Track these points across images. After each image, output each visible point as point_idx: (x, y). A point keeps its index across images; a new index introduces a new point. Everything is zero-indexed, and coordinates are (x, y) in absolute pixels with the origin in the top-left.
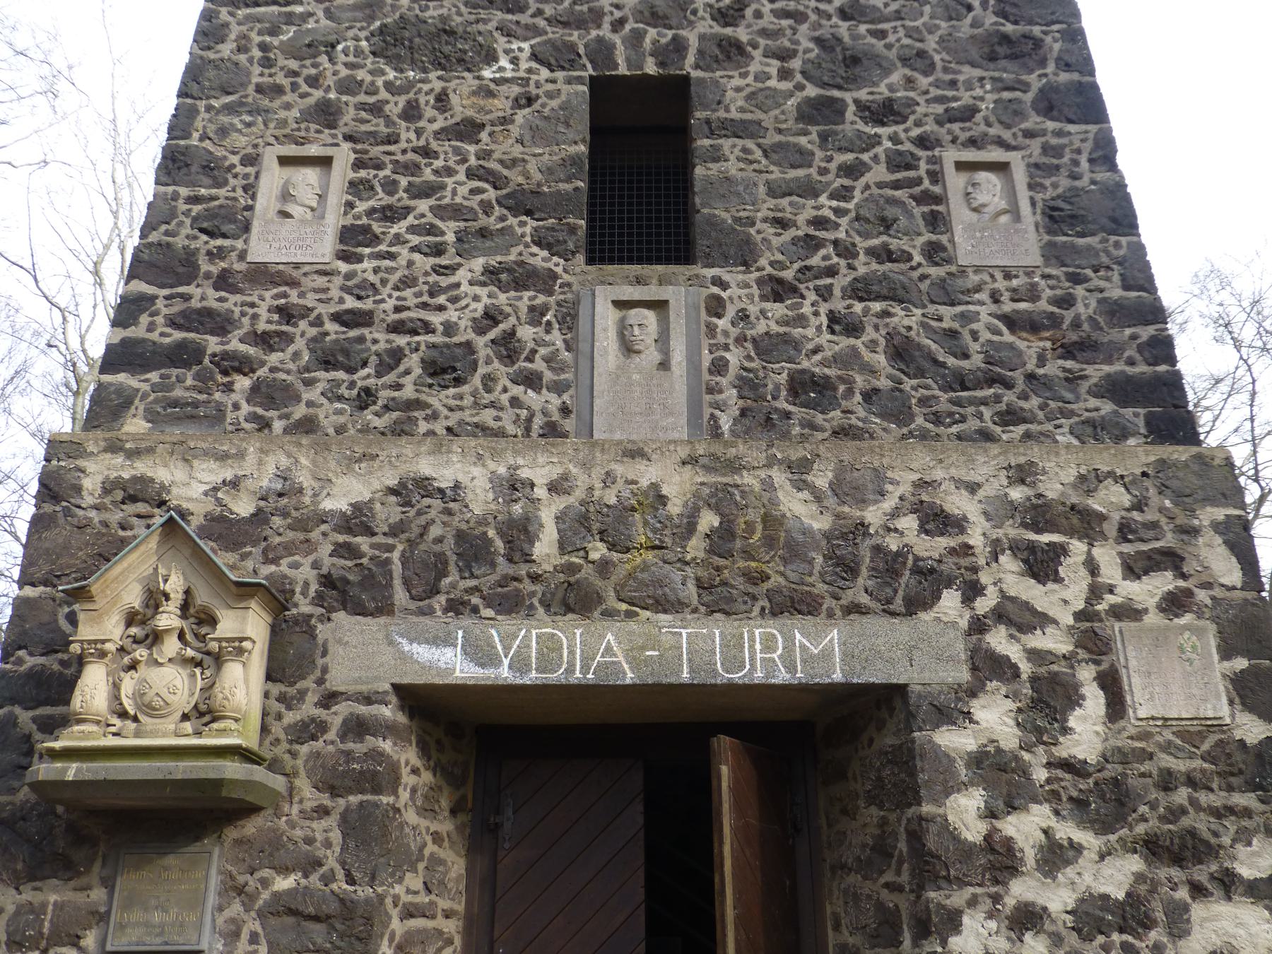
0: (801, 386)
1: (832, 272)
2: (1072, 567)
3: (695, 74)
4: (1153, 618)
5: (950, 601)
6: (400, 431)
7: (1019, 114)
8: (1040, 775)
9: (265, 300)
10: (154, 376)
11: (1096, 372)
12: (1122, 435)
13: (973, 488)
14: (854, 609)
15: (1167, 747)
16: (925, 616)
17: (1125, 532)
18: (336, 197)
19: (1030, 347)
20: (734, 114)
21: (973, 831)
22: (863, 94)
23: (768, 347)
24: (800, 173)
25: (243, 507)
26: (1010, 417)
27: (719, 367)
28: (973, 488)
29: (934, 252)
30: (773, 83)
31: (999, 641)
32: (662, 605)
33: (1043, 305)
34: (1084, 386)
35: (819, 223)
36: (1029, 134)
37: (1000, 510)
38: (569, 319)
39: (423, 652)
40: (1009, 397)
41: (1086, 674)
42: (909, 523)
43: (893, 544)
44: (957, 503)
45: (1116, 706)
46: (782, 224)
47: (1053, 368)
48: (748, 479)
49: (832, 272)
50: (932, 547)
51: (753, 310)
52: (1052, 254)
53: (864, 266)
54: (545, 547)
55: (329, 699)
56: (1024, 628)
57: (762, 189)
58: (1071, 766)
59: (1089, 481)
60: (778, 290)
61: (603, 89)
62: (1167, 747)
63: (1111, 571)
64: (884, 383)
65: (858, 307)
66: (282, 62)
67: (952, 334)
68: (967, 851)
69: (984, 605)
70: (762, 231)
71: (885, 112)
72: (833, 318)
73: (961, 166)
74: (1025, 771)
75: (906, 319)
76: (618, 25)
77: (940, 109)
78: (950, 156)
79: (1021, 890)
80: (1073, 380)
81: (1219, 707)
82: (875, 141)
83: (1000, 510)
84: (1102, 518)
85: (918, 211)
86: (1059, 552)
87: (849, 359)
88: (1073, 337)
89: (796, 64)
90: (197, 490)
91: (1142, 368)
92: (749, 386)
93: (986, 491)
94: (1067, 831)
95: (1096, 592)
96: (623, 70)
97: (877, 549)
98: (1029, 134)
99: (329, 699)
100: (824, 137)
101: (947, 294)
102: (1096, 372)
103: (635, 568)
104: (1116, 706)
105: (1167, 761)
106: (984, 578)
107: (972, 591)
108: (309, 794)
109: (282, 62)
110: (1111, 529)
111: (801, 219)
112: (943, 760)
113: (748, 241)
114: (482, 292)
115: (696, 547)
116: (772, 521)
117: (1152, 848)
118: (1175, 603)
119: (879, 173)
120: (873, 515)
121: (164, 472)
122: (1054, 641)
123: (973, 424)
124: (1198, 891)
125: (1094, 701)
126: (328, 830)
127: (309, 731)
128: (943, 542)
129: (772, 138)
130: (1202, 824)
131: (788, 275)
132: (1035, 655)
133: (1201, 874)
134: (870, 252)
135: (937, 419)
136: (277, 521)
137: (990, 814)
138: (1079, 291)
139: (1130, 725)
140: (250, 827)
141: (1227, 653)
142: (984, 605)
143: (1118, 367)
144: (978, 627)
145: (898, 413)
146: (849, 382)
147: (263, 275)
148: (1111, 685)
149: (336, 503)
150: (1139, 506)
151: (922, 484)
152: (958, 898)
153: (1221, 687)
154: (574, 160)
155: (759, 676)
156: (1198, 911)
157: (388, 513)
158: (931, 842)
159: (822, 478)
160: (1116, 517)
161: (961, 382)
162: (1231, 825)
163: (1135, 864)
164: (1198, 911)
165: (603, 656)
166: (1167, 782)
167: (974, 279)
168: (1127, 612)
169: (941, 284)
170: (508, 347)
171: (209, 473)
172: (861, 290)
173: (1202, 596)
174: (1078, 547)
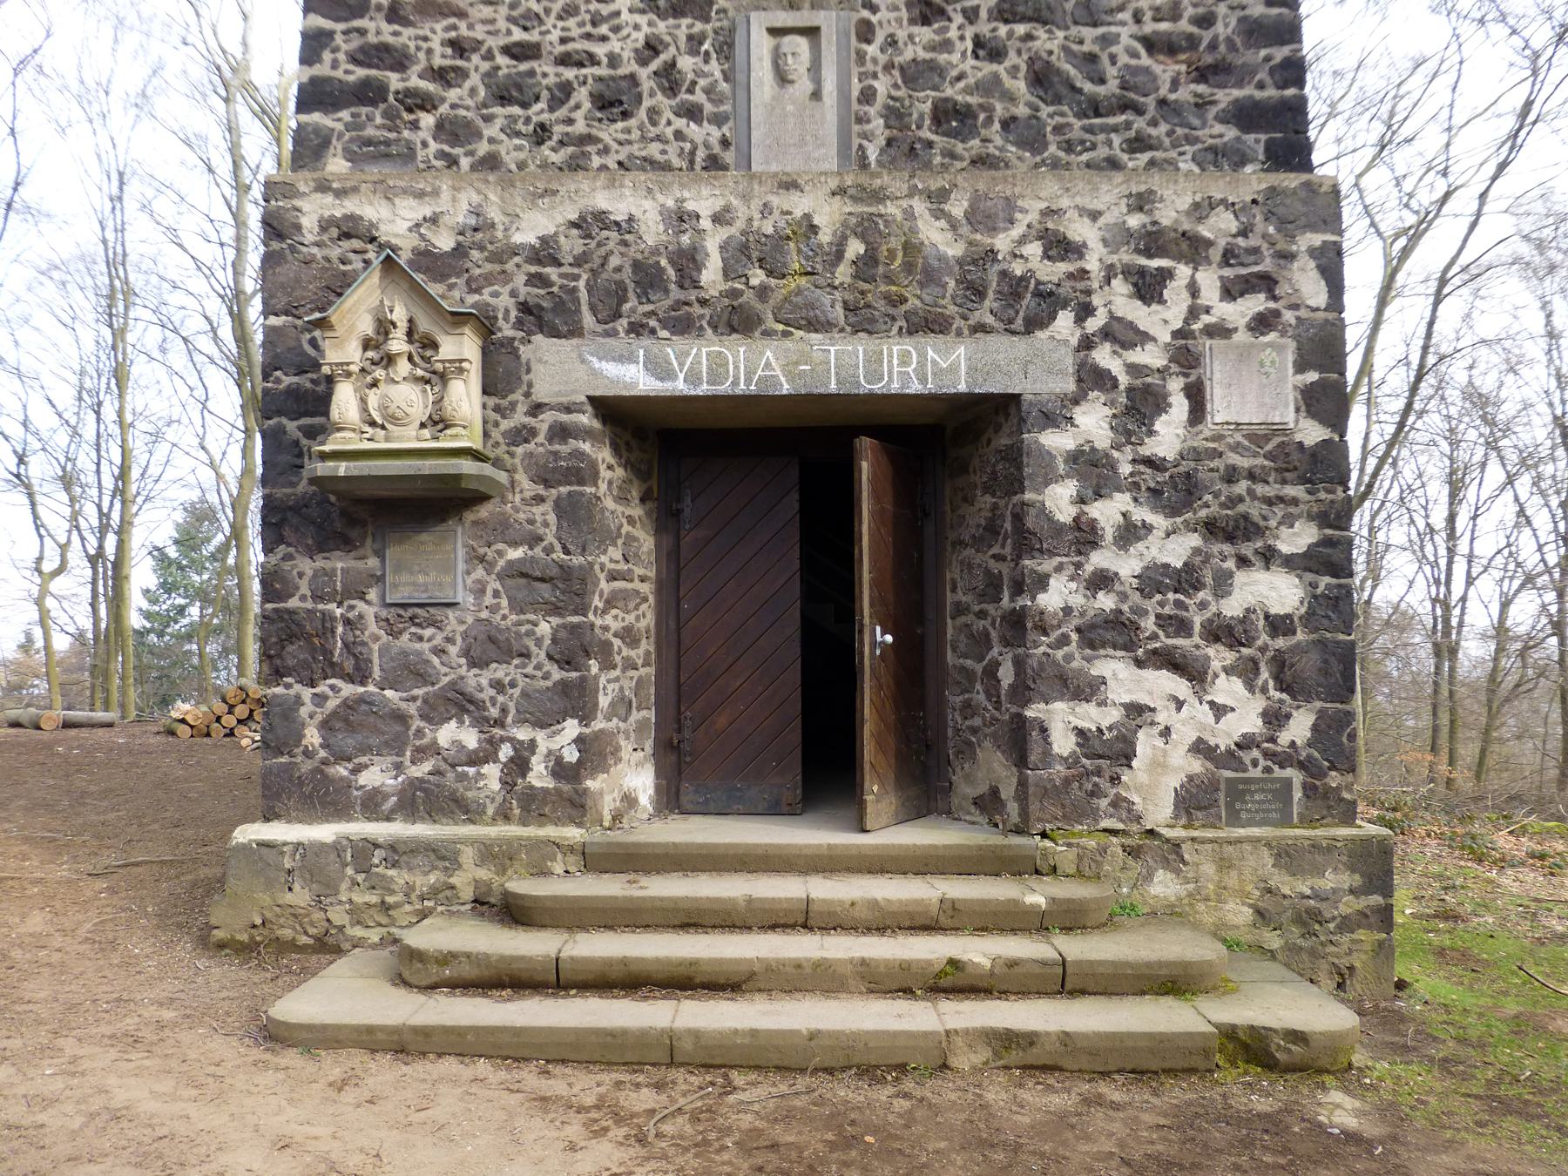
6: (575, 165)
14: (981, 328)
26: (1138, 144)
32: (816, 325)
38: (726, 48)
39: (611, 369)
55: (536, 409)
79: (1098, 560)
95: (1193, 313)
99: (536, 409)
108: (527, 486)
115: (843, 273)
120: (1002, 243)
124: (1243, 562)
125: (1179, 407)
126: (545, 513)
127: (522, 435)
133: (1247, 549)
140: (484, 511)
142: (1093, 324)
144: (1087, 344)
149: (526, 236)
157: (571, 245)
170: (669, 79)
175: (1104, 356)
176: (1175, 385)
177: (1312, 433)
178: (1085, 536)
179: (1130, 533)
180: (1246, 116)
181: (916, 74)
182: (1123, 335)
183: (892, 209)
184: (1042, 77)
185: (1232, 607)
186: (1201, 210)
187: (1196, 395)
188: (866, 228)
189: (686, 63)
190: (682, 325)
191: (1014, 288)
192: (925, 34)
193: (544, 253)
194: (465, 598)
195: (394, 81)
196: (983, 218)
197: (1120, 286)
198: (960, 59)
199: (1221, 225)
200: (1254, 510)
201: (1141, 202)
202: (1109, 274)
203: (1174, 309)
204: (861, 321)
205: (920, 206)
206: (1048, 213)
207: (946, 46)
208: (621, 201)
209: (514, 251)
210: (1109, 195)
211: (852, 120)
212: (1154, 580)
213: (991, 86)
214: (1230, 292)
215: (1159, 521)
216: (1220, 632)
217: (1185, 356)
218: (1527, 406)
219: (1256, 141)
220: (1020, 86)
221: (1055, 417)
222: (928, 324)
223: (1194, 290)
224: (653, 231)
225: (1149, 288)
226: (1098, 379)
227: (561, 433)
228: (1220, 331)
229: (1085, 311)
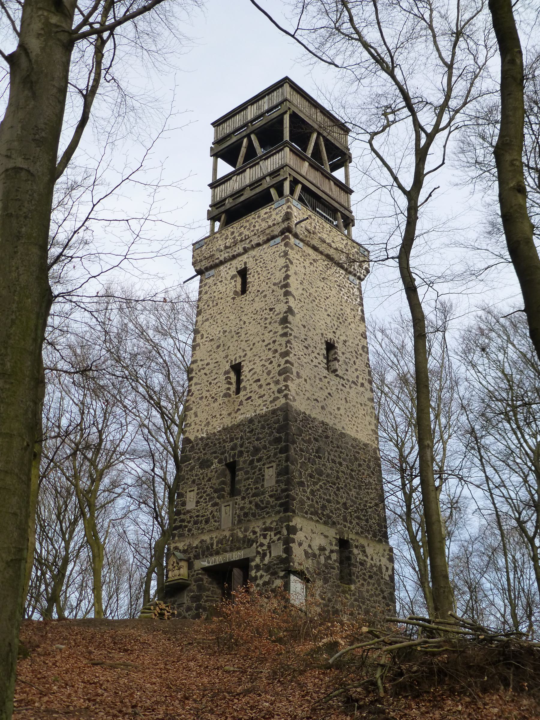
2: (268, 537)
5: (255, 544)
6: (202, 533)
9: (188, 516)
14: (245, 548)
18: (195, 496)
25: (186, 548)
26: (268, 513)
32: (226, 552)
38: (220, 511)
39: (203, 563)
53: (254, 491)
54: (214, 547)
55: (195, 571)
79: (258, 582)
95: (270, 539)
99: (195, 571)
103: (305, 575)
108: (194, 583)
115: (229, 543)
120: (248, 534)
121: (178, 545)
124: (276, 579)
125: (268, 554)
126: (195, 587)
127: (193, 576)
133: (276, 576)
140: (189, 588)
142: (258, 544)
144: (257, 548)
145: (254, 515)
147: (189, 512)
149: (195, 545)
157: (199, 545)
165: (330, 159)
170: (213, 517)
171: (183, 544)
175: (259, 549)
176: (268, 551)
177: (284, 556)
178: (256, 578)
179: (262, 576)
180: (281, 505)
181: (242, 509)
182: (262, 545)
183: (235, 532)
184: (257, 505)
185: (274, 586)
186: (271, 523)
187: (270, 553)
188: (232, 535)
189: (215, 513)
190: (211, 555)
191: (249, 540)
192: (243, 502)
193: (196, 547)
194: (186, 602)
195: (183, 524)
196: (246, 530)
197: (262, 537)
198: (247, 505)
199: (274, 525)
200: (276, 570)
201: (264, 523)
202: (260, 535)
203: (268, 540)
204: (232, 550)
205: (238, 530)
206: (254, 528)
207: (245, 503)
208: (206, 537)
209: (193, 547)
210: (260, 523)
211: (233, 517)
212: (265, 584)
213: (250, 508)
214: (275, 535)
215: (265, 574)
216: (273, 591)
217: (269, 547)
218: (280, 270)
219: (282, 509)
220: (253, 507)
221: (253, 560)
222: (239, 549)
223: (270, 536)
224: (208, 541)
225: (265, 537)
226: (258, 553)
227: (198, 574)
228: (273, 542)
229: (257, 542)
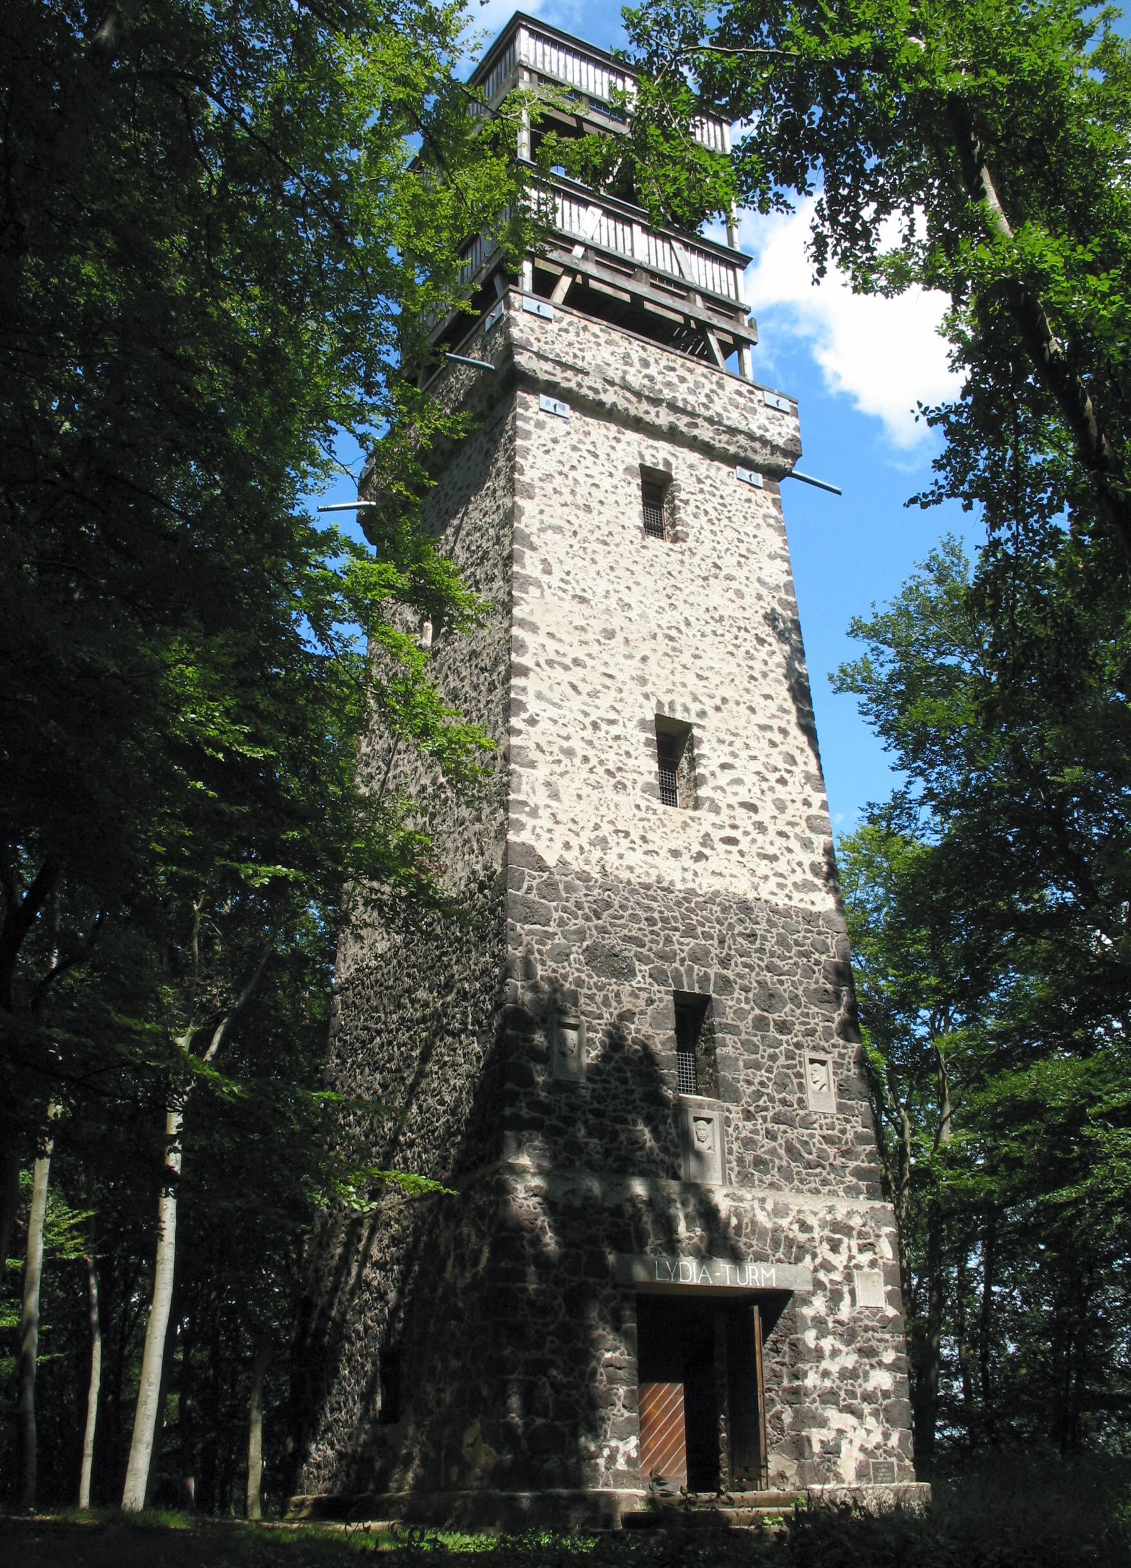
0: (759, 1162)
1: (766, 1109)
2: (843, 1248)
3: (714, 996)
4: (866, 1269)
5: (808, 1258)
7: (831, 1035)
8: (831, 1325)
10: (542, 195)
11: (852, 1164)
12: (859, 1192)
13: (815, 1214)
14: (779, 1261)
15: (867, 1317)
16: (800, 1265)
17: (860, 1235)
19: (832, 1151)
20: (730, 1021)
21: (812, 1344)
22: (775, 1016)
23: (748, 1143)
24: (754, 1056)
26: (825, 1182)
27: (730, 1152)
28: (815, 1214)
29: (801, 1101)
30: (743, 1005)
31: (822, 1275)
33: (836, 1132)
34: (847, 1171)
35: (762, 1084)
36: (834, 1046)
37: (823, 1224)
40: (825, 1173)
41: (846, 1289)
42: (796, 1227)
43: (791, 1236)
44: (812, 1221)
45: (853, 1302)
46: (749, 1083)
47: (839, 1161)
48: (745, 1205)
49: (766, 1109)
50: (802, 1237)
51: (740, 1125)
52: (841, 1108)
53: (779, 1107)
56: (829, 1271)
57: (741, 1063)
58: (839, 1322)
59: (850, 1214)
60: (748, 1116)
61: (678, 996)
62: (867, 1317)
63: (855, 1251)
64: (784, 1163)
65: (776, 1127)
66: (549, 963)
67: (806, 1143)
68: (809, 1350)
69: (818, 1261)
70: (742, 1086)
71: (783, 1027)
72: (768, 1132)
73: (812, 1061)
74: (826, 1323)
75: (792, 1134)
76: (683, 960)
77: (803, 1028)
78: (809, 1054)
79: (825, 1364)
80: (844, 1167)
81: (881, 1302)
82: (780, 1042)
83: (823, 1224)
84: (853, 1229)
85: (795, 1081)
86: (840, 1241)
87: (773, 1152)
88: (844, 1148)
89: (751, 995)
90: (560, 1194)
91: (866, 1164)
92: (740, 1161)
93: (821, 1215)
94: (839, 1345)
95: (851, 1258)
96: (686, 989)
97: (786, 1237)
98: (834, 1046)
100: (763, 1037)
101: (807, 1124)
102: (852, 1164)
104: (853, 1302)
105: (867, 1322)
106: (818, 1251)
107: (814, 1256)
109: (549, 963)
110: (855, 1233)
111: (756, 1081)
112: (803, 1318)
113: (737, 1090)
114: (644, 1105)
116: (753, 1222)
117: (860, 1351)
118: (873, 1264)
119: (782, 1061)
122: (837, 1276)
123: (813, 1185)
124: (872, 1366)
125: (847, 1298)
128: (806, 1236)
129: (744, 1037)
130: (874, 1343)
131: (752, 1109)
132: (831, 1281)
133: (874, 1361)
134: (780, 1100)
135: (801, 1181)
136: (590, 1210)
137: (817, 1338)
138: (848, 1127)
139: (857, 1308)
141: (886, 1283)
143: (858, 1163)
144: (816, 1270)
145: (789, 1178)
146: (772, 1161)
148: (852, 1293)
150: (864, 1225)
151: (799, 1212)
152: (806, 1367)
153: (883, 1296)
154: (670, 1038)
155: (751, 1285)
156: (872, 1373)
158: (800, 1347)
159: (769, 1206)
160: (857, 1228)
161: (809, 1165)
162: (882, 1345)
163: (855, 1357)
164: (872, 1373)
166: (866, 1329)
167: (815, 1117)
168: (858, 1267)
169: (803, 1119)
172: (776, 1120)
173: (880, 1261)
174: (846, 1240)
